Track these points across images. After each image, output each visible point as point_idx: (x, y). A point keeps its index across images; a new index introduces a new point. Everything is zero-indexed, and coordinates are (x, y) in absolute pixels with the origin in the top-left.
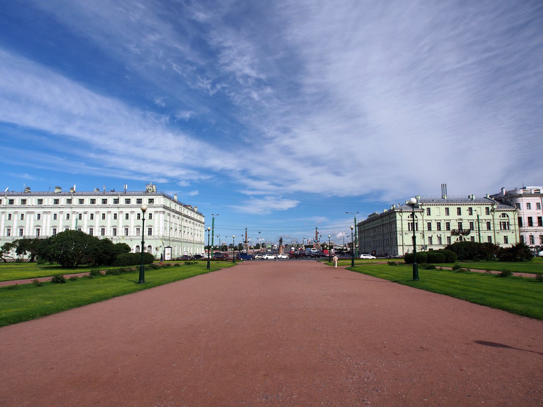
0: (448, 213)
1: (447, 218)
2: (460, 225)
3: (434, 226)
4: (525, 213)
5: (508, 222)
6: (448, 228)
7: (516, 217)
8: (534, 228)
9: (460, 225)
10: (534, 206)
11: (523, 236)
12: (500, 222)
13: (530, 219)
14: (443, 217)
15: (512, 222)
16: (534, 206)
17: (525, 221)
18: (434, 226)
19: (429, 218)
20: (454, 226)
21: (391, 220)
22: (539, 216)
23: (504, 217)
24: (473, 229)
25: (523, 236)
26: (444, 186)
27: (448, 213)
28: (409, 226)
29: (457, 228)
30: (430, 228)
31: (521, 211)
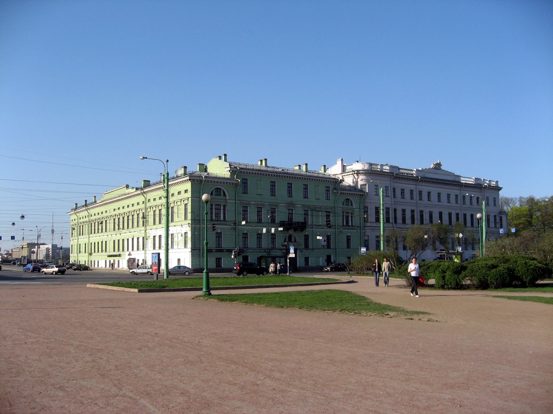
20: (282, 216)
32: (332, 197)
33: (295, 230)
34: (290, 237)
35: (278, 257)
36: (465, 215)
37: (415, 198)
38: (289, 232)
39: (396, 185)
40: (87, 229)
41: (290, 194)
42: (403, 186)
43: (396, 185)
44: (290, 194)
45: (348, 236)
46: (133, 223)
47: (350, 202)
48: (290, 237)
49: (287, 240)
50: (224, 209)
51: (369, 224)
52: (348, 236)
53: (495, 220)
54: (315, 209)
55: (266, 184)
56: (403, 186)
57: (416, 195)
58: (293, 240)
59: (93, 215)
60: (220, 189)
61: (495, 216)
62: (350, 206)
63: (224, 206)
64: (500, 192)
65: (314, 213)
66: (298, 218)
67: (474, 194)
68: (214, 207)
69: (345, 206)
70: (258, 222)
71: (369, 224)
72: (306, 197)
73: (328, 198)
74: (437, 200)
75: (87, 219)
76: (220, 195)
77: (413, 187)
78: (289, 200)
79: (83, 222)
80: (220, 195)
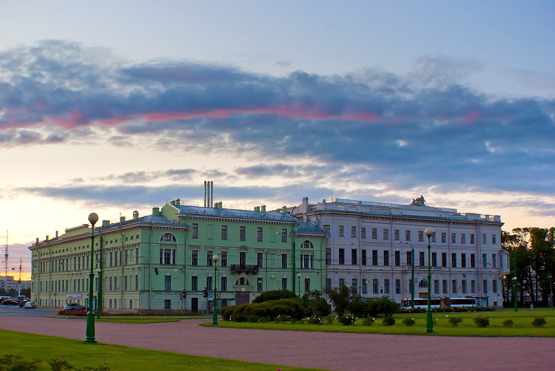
0: (224, 236)
1: (224, 243)
2: (243, 256)
3: (202, 259)
4: (336, 243)
5: (312, 256)
6: (224, 263)
7: (324, 249)
8: (379, 268)
9: (243, 256)
10: (348, 231)
11: (330, 280)
12: (302, 255)
13: (342, 251)
14: (218, 242)
15: (317, 256)
16: (348, 231)
17: (335, 255)
18: (202, 259)
19: (195, 242)
20: (234, 260)
21: (42, 257)
22: (354, 248)
23: (307, 246)
24: (261, 266)
25: (330, 280)
26: (57, 232)
27: (224, 236)
28: (161, 254)
29: (238, 263)
30: (195, 262)
31: (330, 242)
32: (289, 239)
33: (247, 273)
34: (242, 279)
35: (228, 299)
36: (454, 255)
37: (447, 240)
38: (241, 275)
39: (364, 225)
40: (48, 265)
41: (243, 238)
42: (375, 226)
43: (364, 225)
44: (243, 238)
45: (306, 279)
46: (83, 261)
47: (310, 244)
48: (242, 279)
49: (239, 283)
50: (174, 254)
51: (332, 267)
52: (306, 279)
53: (494, 261)
54: (269, 251)
55: (218, 227)
56: (375, 226)
57: (448, 238)
58: (246, 283)
59: (55, 252)
60: (170, 234)
61: (494, 256)
62: (310, 249)
63: (174, 250)
64: (502, 227)
65: (269, 257)
66: (251, 261)
67: (469, 231)
68: (164, 251)
69: (303, 249)
70: (207, 266)
71: (332, 267)
72: (260, 240)
73: (284, 240)
74: (418, 239)
75: (48, 256)
76: (170, 240)
77: (445, 230)
78: (242, 243)
79: (45, 259)
80: (170, 240)
